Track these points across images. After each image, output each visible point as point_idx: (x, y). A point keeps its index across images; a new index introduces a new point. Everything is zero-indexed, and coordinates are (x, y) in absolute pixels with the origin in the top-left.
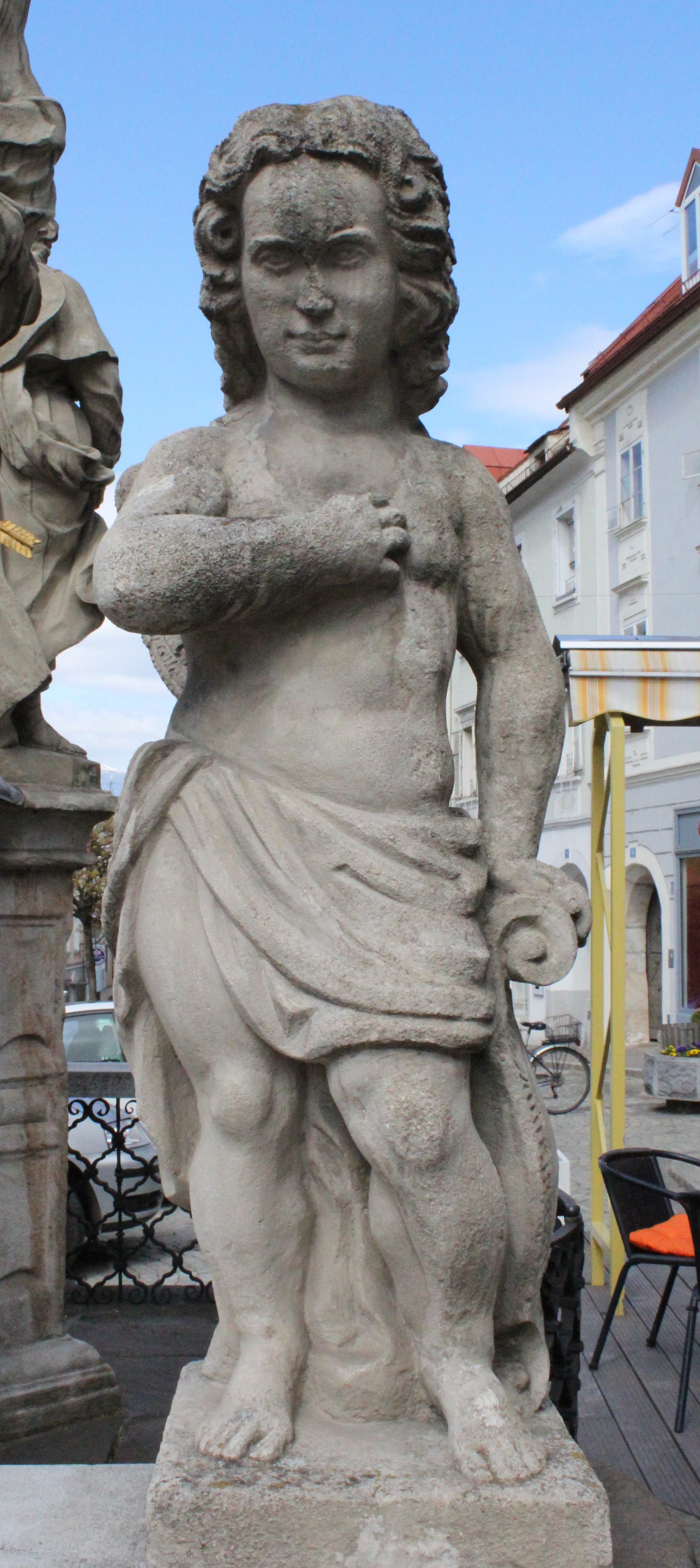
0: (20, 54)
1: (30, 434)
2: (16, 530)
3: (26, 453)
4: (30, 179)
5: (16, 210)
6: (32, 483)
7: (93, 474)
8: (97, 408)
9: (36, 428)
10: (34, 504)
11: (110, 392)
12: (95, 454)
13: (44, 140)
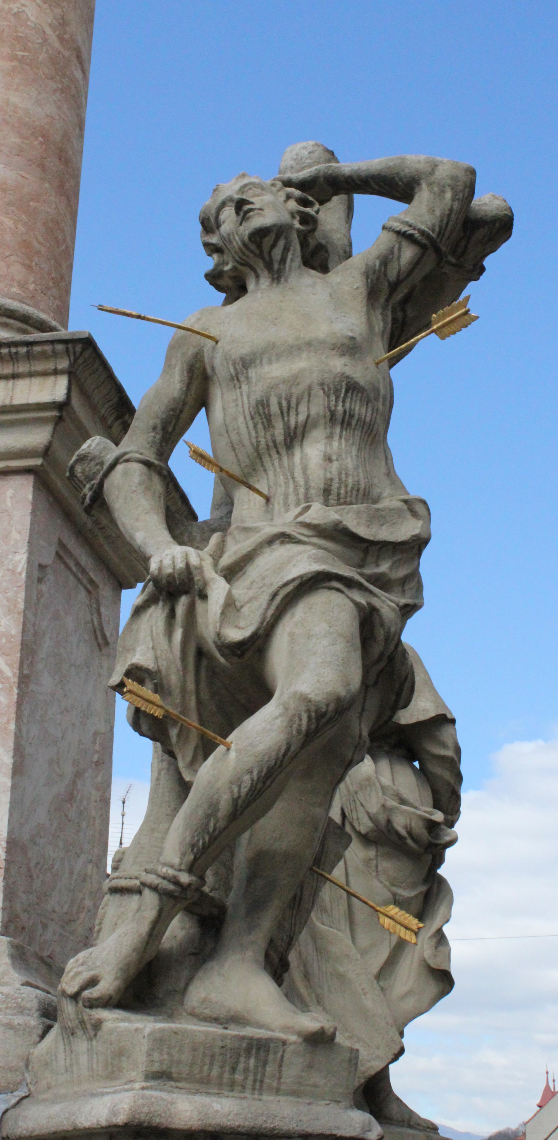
0: (386, 459)
1: (374, 799)
2: (399, 914)
3: (371, 818)
4: (402, 572)
5: (393, 605)
6: (377, 848)
7: (437, 836)
8: (437, 770)
9: (380, 794)
10: (380, 868)
11: (450, 753)
12: (439, 816)
13: (414, 536)
